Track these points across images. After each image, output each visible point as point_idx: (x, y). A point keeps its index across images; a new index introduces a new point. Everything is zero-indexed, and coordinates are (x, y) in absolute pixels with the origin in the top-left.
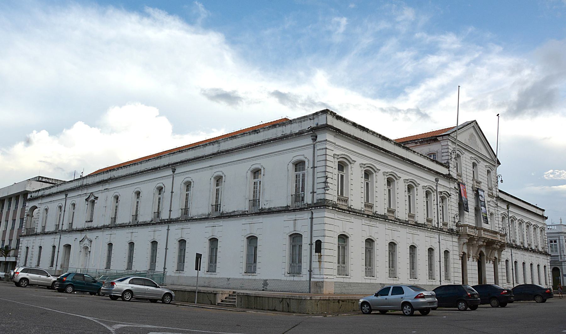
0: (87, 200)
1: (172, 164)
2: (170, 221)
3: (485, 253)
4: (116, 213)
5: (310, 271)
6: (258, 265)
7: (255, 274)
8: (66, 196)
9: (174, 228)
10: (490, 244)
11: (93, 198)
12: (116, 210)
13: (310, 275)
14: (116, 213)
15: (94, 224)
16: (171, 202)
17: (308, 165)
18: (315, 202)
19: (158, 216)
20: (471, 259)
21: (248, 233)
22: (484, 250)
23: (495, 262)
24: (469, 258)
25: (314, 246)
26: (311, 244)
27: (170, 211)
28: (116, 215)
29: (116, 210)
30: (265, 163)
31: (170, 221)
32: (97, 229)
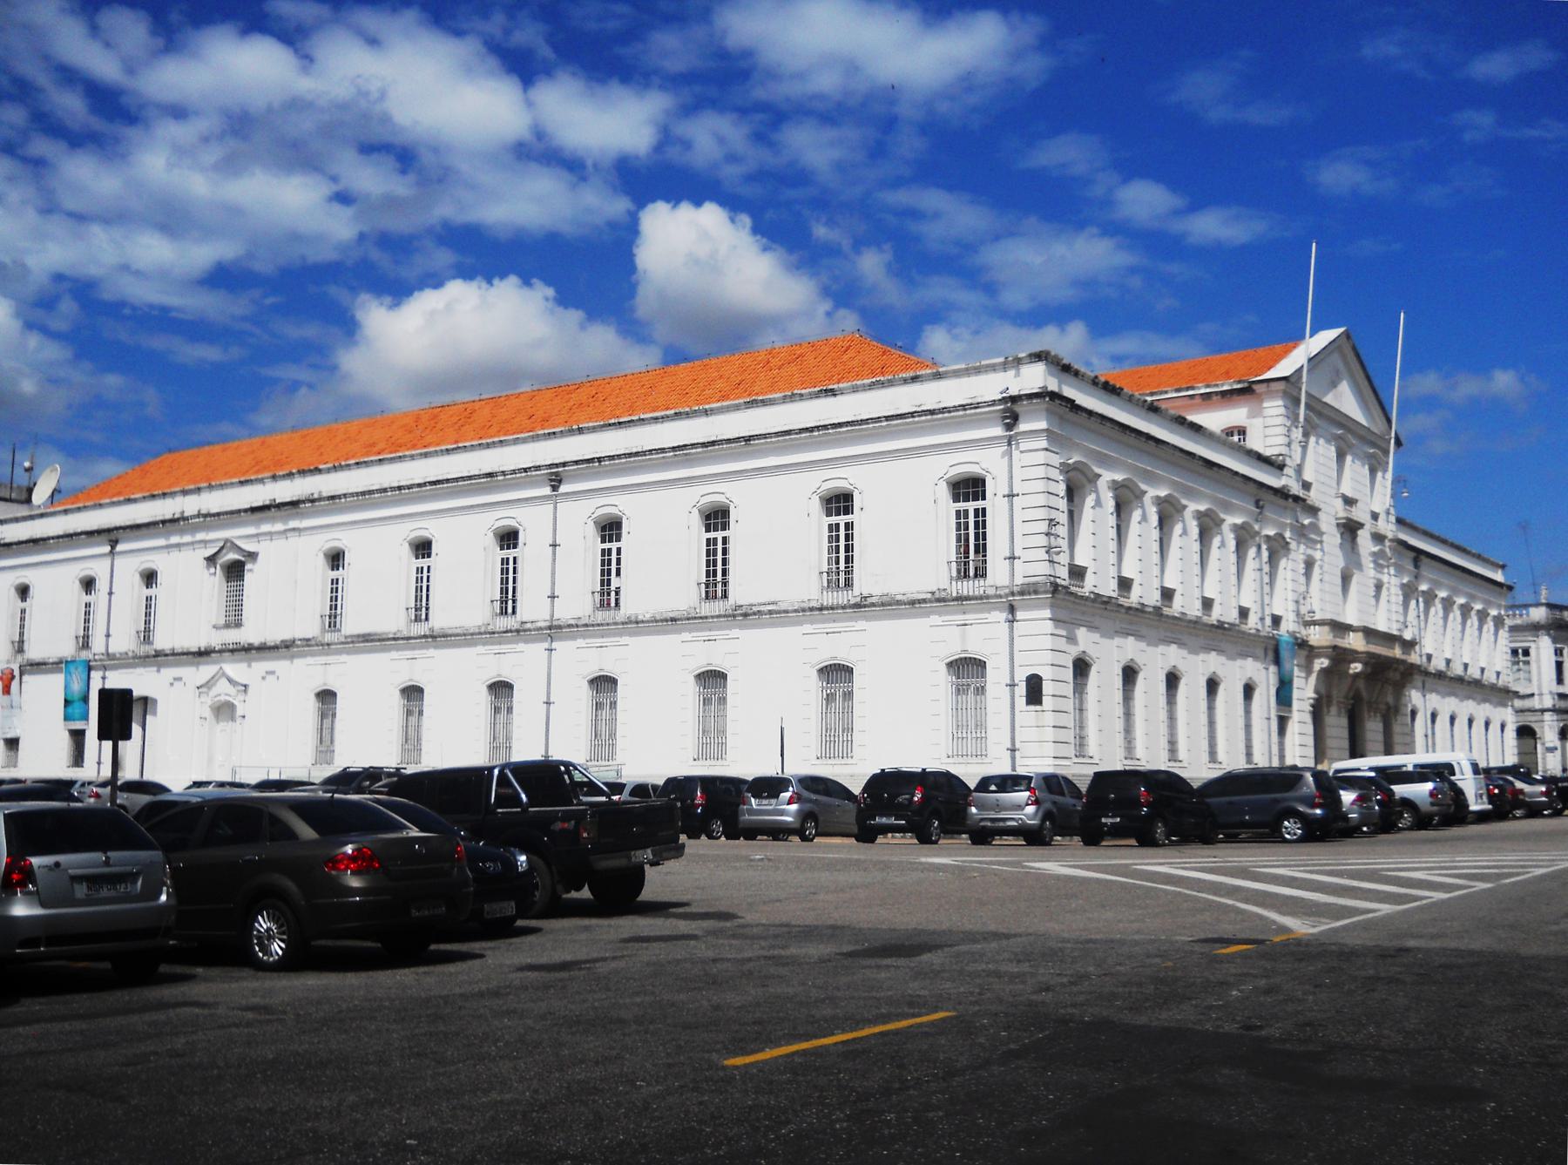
0: (211, 560)
1: (109, 531)
2: (554, 631)
4: (22, 627)
6: (620, 743)
7: (850, 761)
8: (113, 547)
9: (565, 648)
11: (233, 556)
12: (22, 619)
13: (1013, 759)
14: (22, 627)
15: (249, 634)
16: (553, 574)
17: (102, 585)
18: (1019, 580)
19: (20, 650)
20: (1334, 710)
21: (954, 651)
25: (1021, 690)
27: (108, 636)
28: (22, 634)
29: (22, 619)
30: (738, 496)
31: (554, 631)
32: (263, 649)
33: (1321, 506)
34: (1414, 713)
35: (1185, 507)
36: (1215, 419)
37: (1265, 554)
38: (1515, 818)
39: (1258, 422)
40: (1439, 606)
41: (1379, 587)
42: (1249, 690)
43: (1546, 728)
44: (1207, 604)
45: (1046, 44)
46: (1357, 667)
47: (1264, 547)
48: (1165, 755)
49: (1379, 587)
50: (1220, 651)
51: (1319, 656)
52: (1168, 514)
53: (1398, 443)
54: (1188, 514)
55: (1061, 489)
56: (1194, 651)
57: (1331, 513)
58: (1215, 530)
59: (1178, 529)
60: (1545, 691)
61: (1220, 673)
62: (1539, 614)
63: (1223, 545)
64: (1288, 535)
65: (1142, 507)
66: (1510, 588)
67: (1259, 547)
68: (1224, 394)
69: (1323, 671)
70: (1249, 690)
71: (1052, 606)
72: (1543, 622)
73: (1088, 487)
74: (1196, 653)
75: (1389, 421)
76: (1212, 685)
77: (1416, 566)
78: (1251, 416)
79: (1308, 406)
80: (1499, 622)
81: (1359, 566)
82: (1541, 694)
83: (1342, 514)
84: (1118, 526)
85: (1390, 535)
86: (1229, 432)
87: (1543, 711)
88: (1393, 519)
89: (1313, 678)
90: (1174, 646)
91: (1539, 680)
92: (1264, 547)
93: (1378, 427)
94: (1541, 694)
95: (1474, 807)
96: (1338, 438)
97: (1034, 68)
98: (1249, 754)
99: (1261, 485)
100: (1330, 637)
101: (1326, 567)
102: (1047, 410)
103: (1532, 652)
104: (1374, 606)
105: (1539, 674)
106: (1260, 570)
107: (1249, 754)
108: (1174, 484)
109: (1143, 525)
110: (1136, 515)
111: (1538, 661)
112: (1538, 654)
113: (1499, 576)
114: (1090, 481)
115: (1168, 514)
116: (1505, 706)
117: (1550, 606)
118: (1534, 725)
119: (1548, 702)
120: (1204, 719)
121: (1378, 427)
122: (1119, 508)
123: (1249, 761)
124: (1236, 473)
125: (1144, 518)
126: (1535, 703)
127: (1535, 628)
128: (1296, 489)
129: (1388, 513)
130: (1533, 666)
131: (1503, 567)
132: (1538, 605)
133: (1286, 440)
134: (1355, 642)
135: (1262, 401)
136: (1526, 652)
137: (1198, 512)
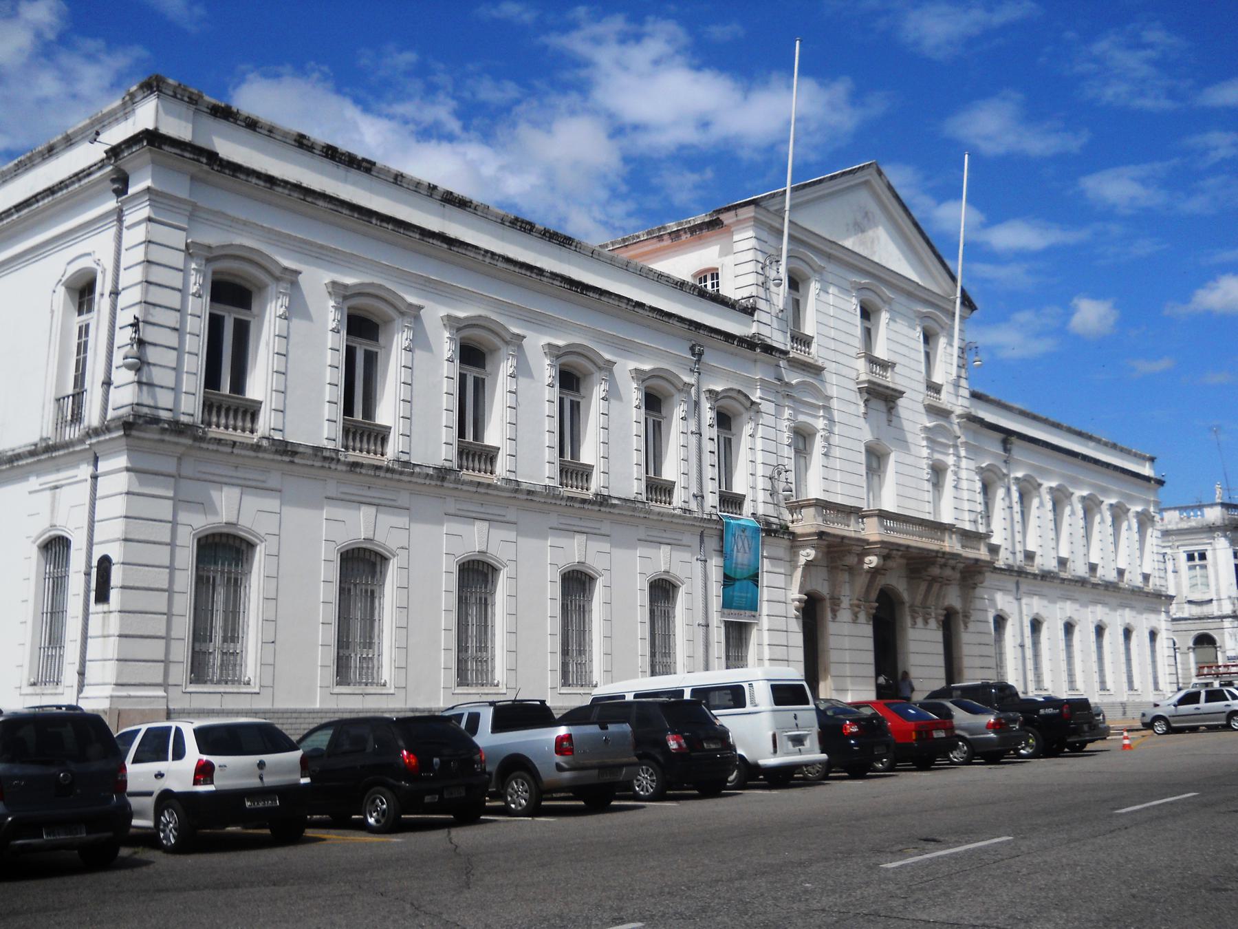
3: (906, 596)
5: (82, 674)
10: (919, 564)
20: (845, 615)
22: (899, 584)
23: (950, 625)
24: (834, 612)
26: (88, 574)
33: (827, 365)
34: (1000, 621)
35: (1040, 485)
36: (683, 264)
37: (1015, 495)
38: (363, 826)
39: (729, 260)
40: (1047, 499)
41: (938, 471)
42: (1153, 635)
43: (1227, 636)
44: (1146, 577)
45: (856, 98)
46: (872, 561)
47: (1014, 488)
48: (1065, 686)
49: (938, 471)
50: (1132, 608)
51: (803, 547)
52: (1059, 499)
53: (967, 303)
54: (1075, 499)
55: (978, 485)
56: (1084, 605)
57: (844, 374)
58: (1096, 510)
59: (1067, 510)
60: (1224, 596)
61: (1076, 617)
62: (1214, 515)
63: (1103, 521)
64: (1152, 509)
65: (1040, 496)
66: (1161, 483)
67: (1009, 490)
68: (693, 230)
69: (808, 564)
70: (1153, 635)
71: (131, 450)
72: (1219, 523)
73: (1035, 493)
74: (1115, 610)
75: (954, 279)
76: (1069, 628)
77: (1006, 450)
78: (725, 252)
79: (791, 237)
80: (1145, 521)
81: (903, 443)
82: (1219, 600)
83: (863, 377)
84: (1055, 520)
85: (959, 411)
86: (702, 276)
87: (1222, 618)
88: (966, 393)
89: (798, 573)
90: (1069, 603)
91: (1217, 584)
92: (1014, 488)
93: (935, 283)
94: (1219, 600)
95: (463, 794)
96: (861, 288)
97: (847, 120)
98: (1072, 681)
99: (698, 326)
100: (820, 521)
101: (835, 440)
102: (153, 162)
103: (1209, 555)
104: (927, 491)
105: (1217, 579)
106: (1011, 508)
107: (1072, 681)
108: (1063, 476)
109: (1041, 508)
110: (1035, 502)
111: (1215, 564)
112: (1215, 558)
113: (1146, 470)
114: (1000, 479)
115: (1059, 499)
116: (1158, 612)
117: (1225, 505)
118: (1211, 633)
119: (1227, 609)
120: (1123, 658)
121: (935, 283)
122: (1022, 496)
123: (1072, 688)
124: (640, 305)
125: (1042, 504)
126: (1213, 609)
127: (1211, 529)
128: (779, 339)
129: (957, 385)
130: (1210, 569)
131: (1152, 460)
132: (1212, 505)
133: (761, 279)
134: (871, 531)
135: (732, 234)
136: (1203, 556)
137: (1051, 488)
